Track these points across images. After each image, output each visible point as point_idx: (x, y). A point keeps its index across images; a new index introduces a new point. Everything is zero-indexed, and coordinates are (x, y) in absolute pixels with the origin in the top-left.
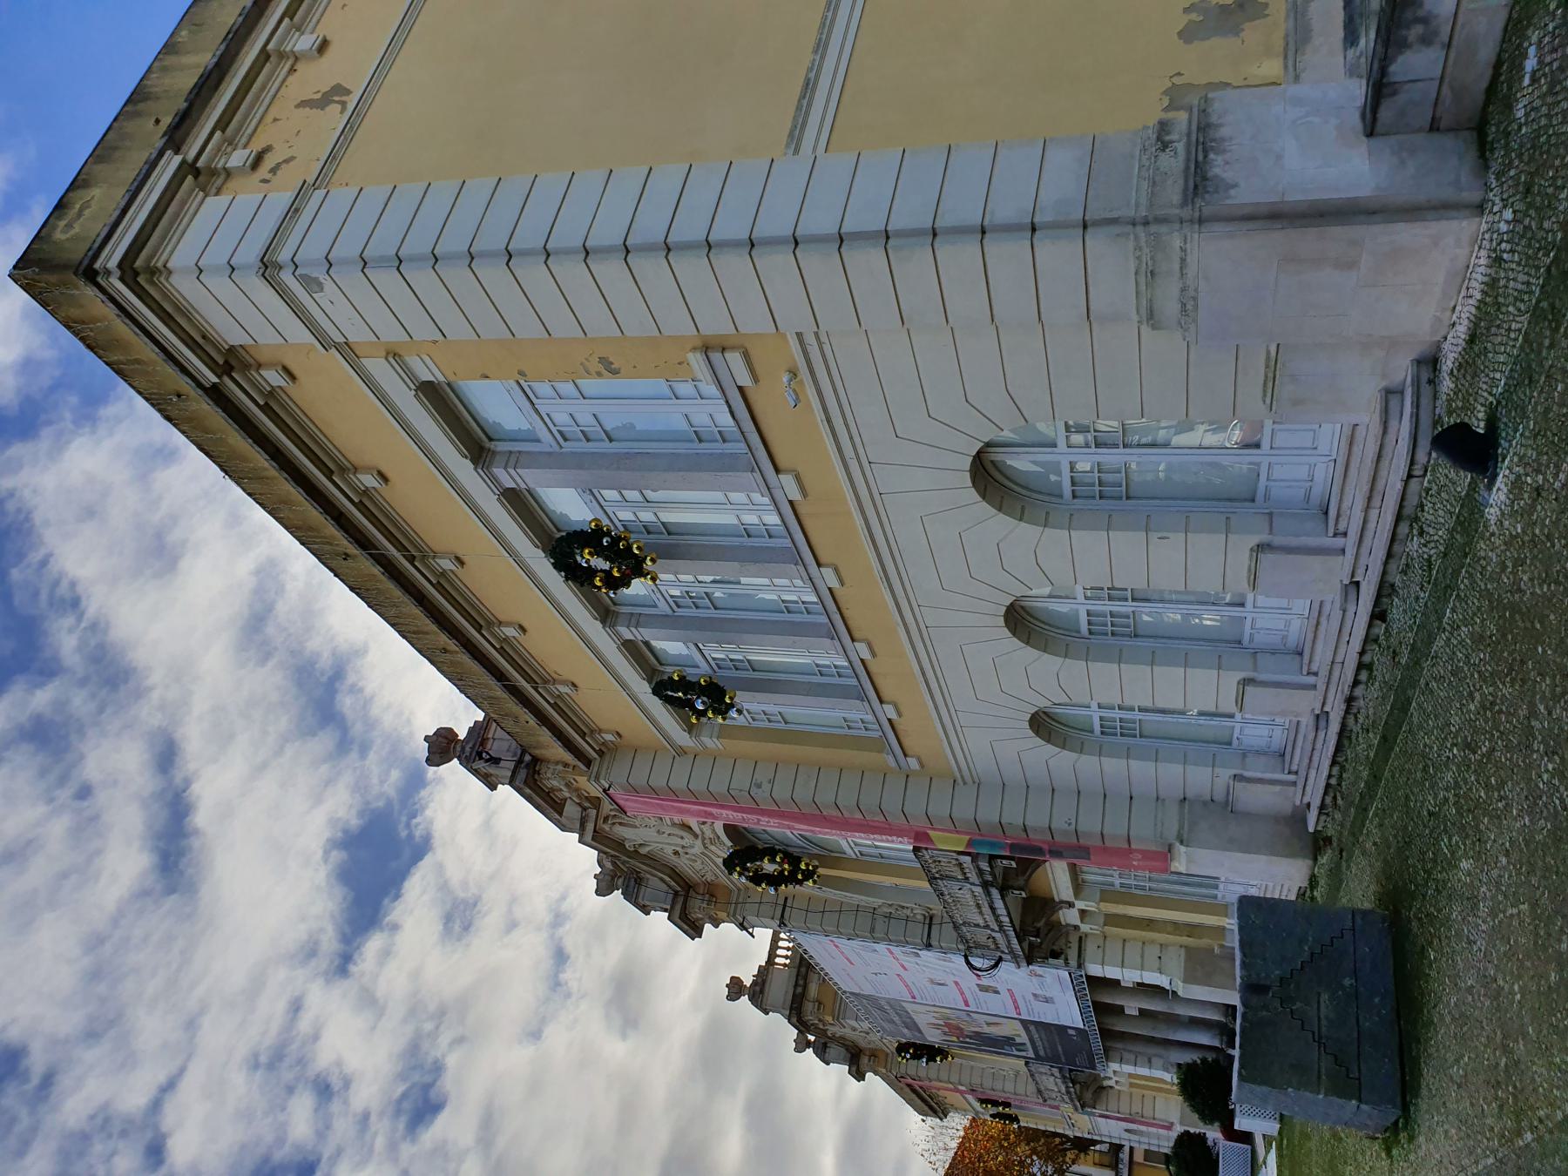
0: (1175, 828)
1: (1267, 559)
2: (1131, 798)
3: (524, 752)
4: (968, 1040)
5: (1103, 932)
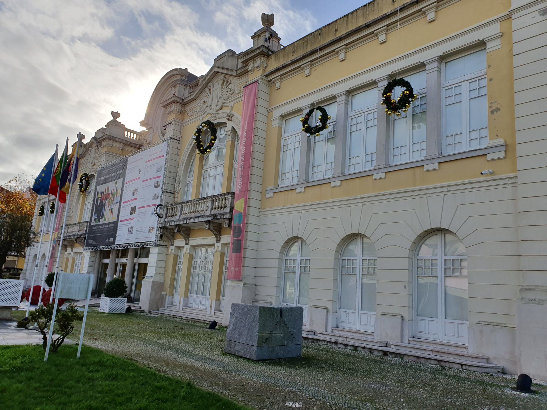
0: (248, 283)
1: (399, 320)
2: (255, 268)
3: (273, 52)
4: (99, 201)
5: (170, 254)
